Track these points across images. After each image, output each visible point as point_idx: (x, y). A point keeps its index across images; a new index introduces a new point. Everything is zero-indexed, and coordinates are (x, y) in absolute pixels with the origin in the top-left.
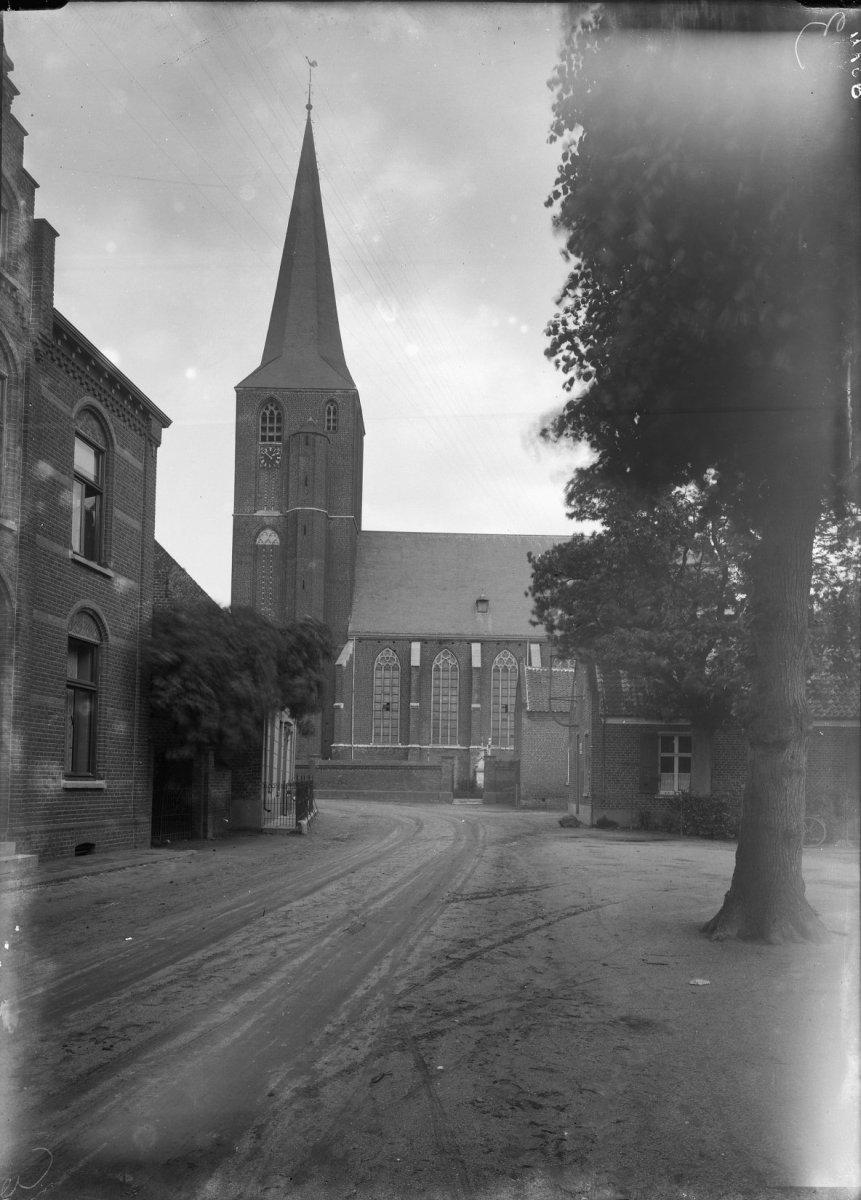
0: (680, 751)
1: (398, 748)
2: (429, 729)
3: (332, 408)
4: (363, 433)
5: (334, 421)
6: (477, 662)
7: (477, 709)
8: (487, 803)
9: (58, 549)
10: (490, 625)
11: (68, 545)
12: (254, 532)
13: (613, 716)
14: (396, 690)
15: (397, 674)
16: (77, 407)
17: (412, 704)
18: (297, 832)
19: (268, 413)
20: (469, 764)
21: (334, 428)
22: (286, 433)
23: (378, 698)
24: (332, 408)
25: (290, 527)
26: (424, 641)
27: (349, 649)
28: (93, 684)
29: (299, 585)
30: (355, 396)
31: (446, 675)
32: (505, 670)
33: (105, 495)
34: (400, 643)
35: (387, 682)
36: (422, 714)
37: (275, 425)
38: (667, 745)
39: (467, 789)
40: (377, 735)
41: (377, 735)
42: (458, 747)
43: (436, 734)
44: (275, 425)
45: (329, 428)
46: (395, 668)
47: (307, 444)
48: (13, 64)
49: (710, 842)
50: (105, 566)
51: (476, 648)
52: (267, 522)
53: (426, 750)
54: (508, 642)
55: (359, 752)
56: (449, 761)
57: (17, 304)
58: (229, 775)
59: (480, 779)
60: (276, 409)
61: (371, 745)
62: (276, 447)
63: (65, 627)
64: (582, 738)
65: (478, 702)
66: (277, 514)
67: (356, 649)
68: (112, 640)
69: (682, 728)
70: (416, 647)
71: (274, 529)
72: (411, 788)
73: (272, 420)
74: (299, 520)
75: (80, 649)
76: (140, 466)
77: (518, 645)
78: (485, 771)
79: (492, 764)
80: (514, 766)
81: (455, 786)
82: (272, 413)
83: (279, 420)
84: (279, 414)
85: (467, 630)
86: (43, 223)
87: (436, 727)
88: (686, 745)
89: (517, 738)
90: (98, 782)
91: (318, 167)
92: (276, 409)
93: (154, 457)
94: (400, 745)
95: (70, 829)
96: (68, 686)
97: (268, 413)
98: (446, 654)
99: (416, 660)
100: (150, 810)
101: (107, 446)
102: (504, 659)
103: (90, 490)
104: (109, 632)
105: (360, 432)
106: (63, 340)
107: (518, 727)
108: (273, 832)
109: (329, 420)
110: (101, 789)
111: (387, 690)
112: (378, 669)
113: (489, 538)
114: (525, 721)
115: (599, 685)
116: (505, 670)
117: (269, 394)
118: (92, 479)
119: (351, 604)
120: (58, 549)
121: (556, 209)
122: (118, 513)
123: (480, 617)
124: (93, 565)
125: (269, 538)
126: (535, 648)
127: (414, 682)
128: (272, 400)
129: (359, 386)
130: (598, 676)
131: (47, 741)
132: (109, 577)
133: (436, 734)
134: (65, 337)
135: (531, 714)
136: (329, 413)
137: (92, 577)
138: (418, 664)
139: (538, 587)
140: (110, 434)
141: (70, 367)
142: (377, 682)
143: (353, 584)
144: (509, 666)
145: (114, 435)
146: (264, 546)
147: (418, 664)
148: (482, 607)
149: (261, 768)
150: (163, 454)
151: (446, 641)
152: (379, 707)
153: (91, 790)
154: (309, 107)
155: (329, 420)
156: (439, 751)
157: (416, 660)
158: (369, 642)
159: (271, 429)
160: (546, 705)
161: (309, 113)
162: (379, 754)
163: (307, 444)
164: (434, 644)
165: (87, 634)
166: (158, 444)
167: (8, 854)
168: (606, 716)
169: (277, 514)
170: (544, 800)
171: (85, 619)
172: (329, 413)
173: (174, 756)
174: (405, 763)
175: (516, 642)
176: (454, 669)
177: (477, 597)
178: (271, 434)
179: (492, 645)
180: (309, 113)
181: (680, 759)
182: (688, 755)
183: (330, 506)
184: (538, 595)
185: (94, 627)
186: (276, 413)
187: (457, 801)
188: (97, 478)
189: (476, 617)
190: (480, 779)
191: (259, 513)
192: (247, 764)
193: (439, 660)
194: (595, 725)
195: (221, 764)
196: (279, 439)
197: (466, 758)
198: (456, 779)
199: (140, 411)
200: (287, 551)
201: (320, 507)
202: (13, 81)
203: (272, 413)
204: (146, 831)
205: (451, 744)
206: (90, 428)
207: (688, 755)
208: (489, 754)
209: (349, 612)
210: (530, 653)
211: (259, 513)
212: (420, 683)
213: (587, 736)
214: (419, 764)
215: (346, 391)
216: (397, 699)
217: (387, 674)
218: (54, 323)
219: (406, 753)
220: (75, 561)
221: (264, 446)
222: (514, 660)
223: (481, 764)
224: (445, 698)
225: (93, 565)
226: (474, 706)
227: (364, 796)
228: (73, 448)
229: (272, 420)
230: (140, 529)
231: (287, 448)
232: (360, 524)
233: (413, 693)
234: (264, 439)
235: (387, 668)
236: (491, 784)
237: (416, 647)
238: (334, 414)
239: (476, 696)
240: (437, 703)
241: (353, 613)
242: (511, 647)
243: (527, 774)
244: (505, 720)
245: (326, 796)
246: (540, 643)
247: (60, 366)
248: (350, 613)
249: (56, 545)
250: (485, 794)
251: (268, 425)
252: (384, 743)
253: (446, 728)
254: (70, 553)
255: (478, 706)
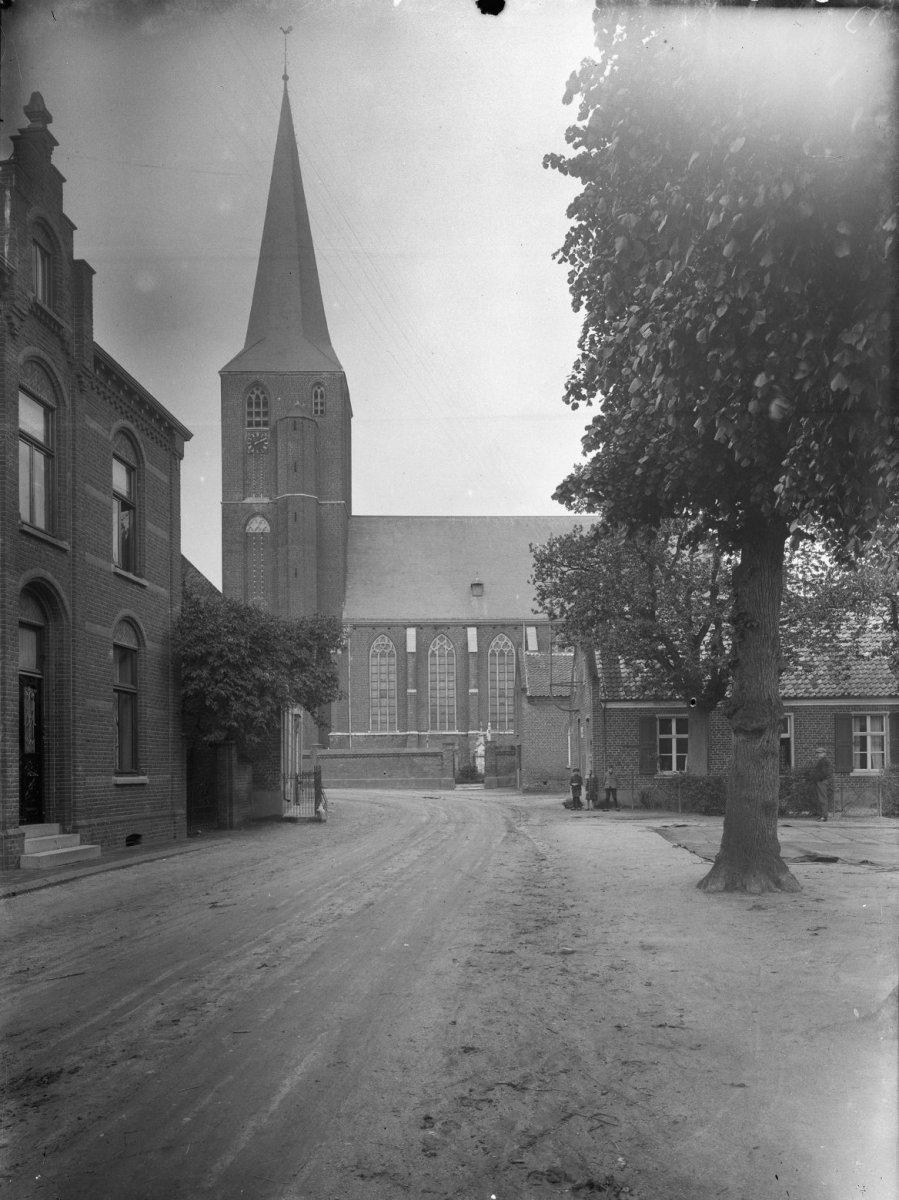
0: (678, 732)
1: (396, 736)
2: (427, 716)
4: (350, 415)
5: (322, 404)
6: (473, 647)
7: (475, 694)
8: (489, 787)
9: (101, 563)
10: (486, 609)
11: (109, 558)
12: (243, 522)
13: (613, 701)
14: (393, 677)
15: (394, 660)
16: (113, 432)
17: (409, 691)
18: (318, 820)
19: (253, 397)
20: (469, 750)
21: (322, 411)
22: (272, 419)
23: (375, 685)
25: (279, 514)
26: (419, 626)
28: (132, 687)
29: (292, 572)
30: (343, 379)
31: (442, 661)
32: (502, 654)
33: (138, 510)
34: (395, 629)
35: (384, 669)
36: (419, 702)
37: (262, 409)
38: (666, 729)
39: (468, 776)
40: (374, 722)
41: (374, 722)
42: (457, 732)
43: (434, 722)
44: (262, 409)
45: (316, 412)
46: (391, 655)
47: (295, 429)
48: (51, 117)
49: (790, 9)
50: (141, 576)
51: (472, 633)
52: (256, 509)
53: (425, 736)
54: (503, 626)
55: (358, 742)
57: (63, 341)
58: (250, 768)
59: (480, 764)
60: (263, 393)
61: (369, 733)
62: (264, 432)
63: (110, 636)
64: (583, 722)
65: (475, 687)
66: (266, 500)
68: (148, 644)
69: (680, 710)
70: (411, 633)
71: (263, 516)
73: (258, 404)
74: (290, 507)
75: (125, 654)
76: (165, 478)
77: (515, 627)
79: (493, 750)
80: (515, 751)
82: (258, 397)
83: (266, 404)
84: (265, 398)
85: (462, 614)
86: (82, 263)
87: (434, 713)
88: (683, 727)
89: (517, 721)
90: (141, 778)
91: (294, 123)
92: (263, 393)
93: (178, 470)
94: (398, 733)
95: (121, 822)
96: (115, 690)
97: (253, 397)
98: (441, 639)
99: (411, 647)
100: (185, 803)
101: (138, 463)
102: (502, 642)
103: (126, 506)
104: (146, 637)
105: (347, 413)
106: (145, 409)
107: (518, 709)
108: (292, 820)
109: (316, 404)
110: (143, 785)
111: (383, 677)
112: (375, 656)
113: (482, 520)
114: (525, 705)
115: (599, 671)
116: (502, 654)
117: (253, 378)
118: (125, 494)
119: (344, 592)
120: (101, 563)
121: (602, 404)
122: (150, 526)
123: (475, 601)
124: (131, 576)
125: (258, 525)
126: (531, 632)
127: (412, 669)
128: (257, 384)
129: (345, 369)
130: (597, 662)
131: (99, 742)
132: (143, 586)
133: (434, 722)
134: (114, 378)
135: (531, 699)
136: (316, 397)
137: (130, 588)
138: (414, 650)
139: (540, 576)
140: (141, 452)
141: (108, 394)
142: (373, 670)
143: (345, 570)
144: (506, 650)
145: (144, 453)
146: (255, 534)
147: (414, 650)
148: (477, 590)
149: (279, 760)
150: (185, 466)
151: (442, 626)
152: (375, 694)
153: (136, 785)
154: (286, 78)
155: (316, 404)
156: (438, 737)
157: (411, 647)
158: (363, 629)
159: (258, 414)
160: (547, 689)
161: (286, 84)
162: (377, 742)
164: (430, 629)
165: (129, 642)
166: (181, 456)
167: (75, 845)
168: (606, 701)
169: (266, 500)
170: (545, 783)
171: (126, 628)
172: (316, 397)
173: (233, 752)
174: (407, 750)
175: (512, 625)
176: (450, 655)
177: (470, 583)
178: (258, 419)
179: (488, 629)
180: (286, 84)
181: (678, 740)
182: (685, 736)
183: (319, 492)
184: (539, 583)
185: (132, 633)
186: (262, 397)
188: (129, 493)
189: (471, 602)
190: (480, 764)
191: (248, 500)
192: (265, 755)
193: (436, 646)
194: (595, 710)
195: (244, 759)
196: (266, 424)
197: (466, 742)
198: (457, 767)
199: (114, 382)
200: (277, 539)
201: (307, 493)
203: (258, 397)
204: (182, 822)
205: (449, 729)
206: (126, 453)
207: (685, 736)
208: (489, 739)
209: (342, 599)
210: (526, 642)
211: (248, 500)
212: (417, 669)
213: (588, 720)
214: (421, 751)
215: (333, 373)
216: (394, 686)
217: (384, 661)
218: (95, 356)
219: (405, 740)
220: (116, 574)
221: (252, 432)
222: (510, 644)
223: (481, 750)
224: (443, 686)
225: (131, 576)
226: (471, 691)
228: (111, 468)
229: (258, 404)
230: (167, 538)
231: (274, 432)
232: (350, 509)
233: (410, 680)
234: (250, 424)
235: (383, 655)
236: (491, 769)
237: (411, 633)
239: (473, 682)
240: (434, 689)
241: (347, 600)
243: (529, 757)
244: (502, 704)
245: (338, 785)
246: (537, 625)
247: (99, 393)
248: (344, 600)
249: (100, 561)
250: (487, 779)
251: (254, 409)
252: (382, 730)
253: (444, 713)
254: (113, 565)
255: (476, 691)
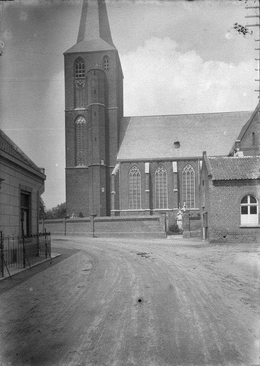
3: (106, 60)
8: (185, 237)
19: (78, 64)
21: (108, 68)
24: (106, 60)
27: (117, 166)
34: (140, 162)
47: (95, 74)
52: (80, 113)
56: (164, 215)
67: (120, 167)
72: (143, 231)
78: (183, 220)
81: (167, 230)
83: (83, 68)
85: (169, 156)
97: (78, 64)
98: (161, 167)
144: (190, 171)
163: (95, 74)
170: (225, 237)
178: (80, 74)
187: (169, 237)
191: (76, 109)
202: (148, 163)
203: (80, 64)
222: (192, 168)
227: (118, 235)
237: (147, 165)
238: (108, 62)
242: (191, 163)
